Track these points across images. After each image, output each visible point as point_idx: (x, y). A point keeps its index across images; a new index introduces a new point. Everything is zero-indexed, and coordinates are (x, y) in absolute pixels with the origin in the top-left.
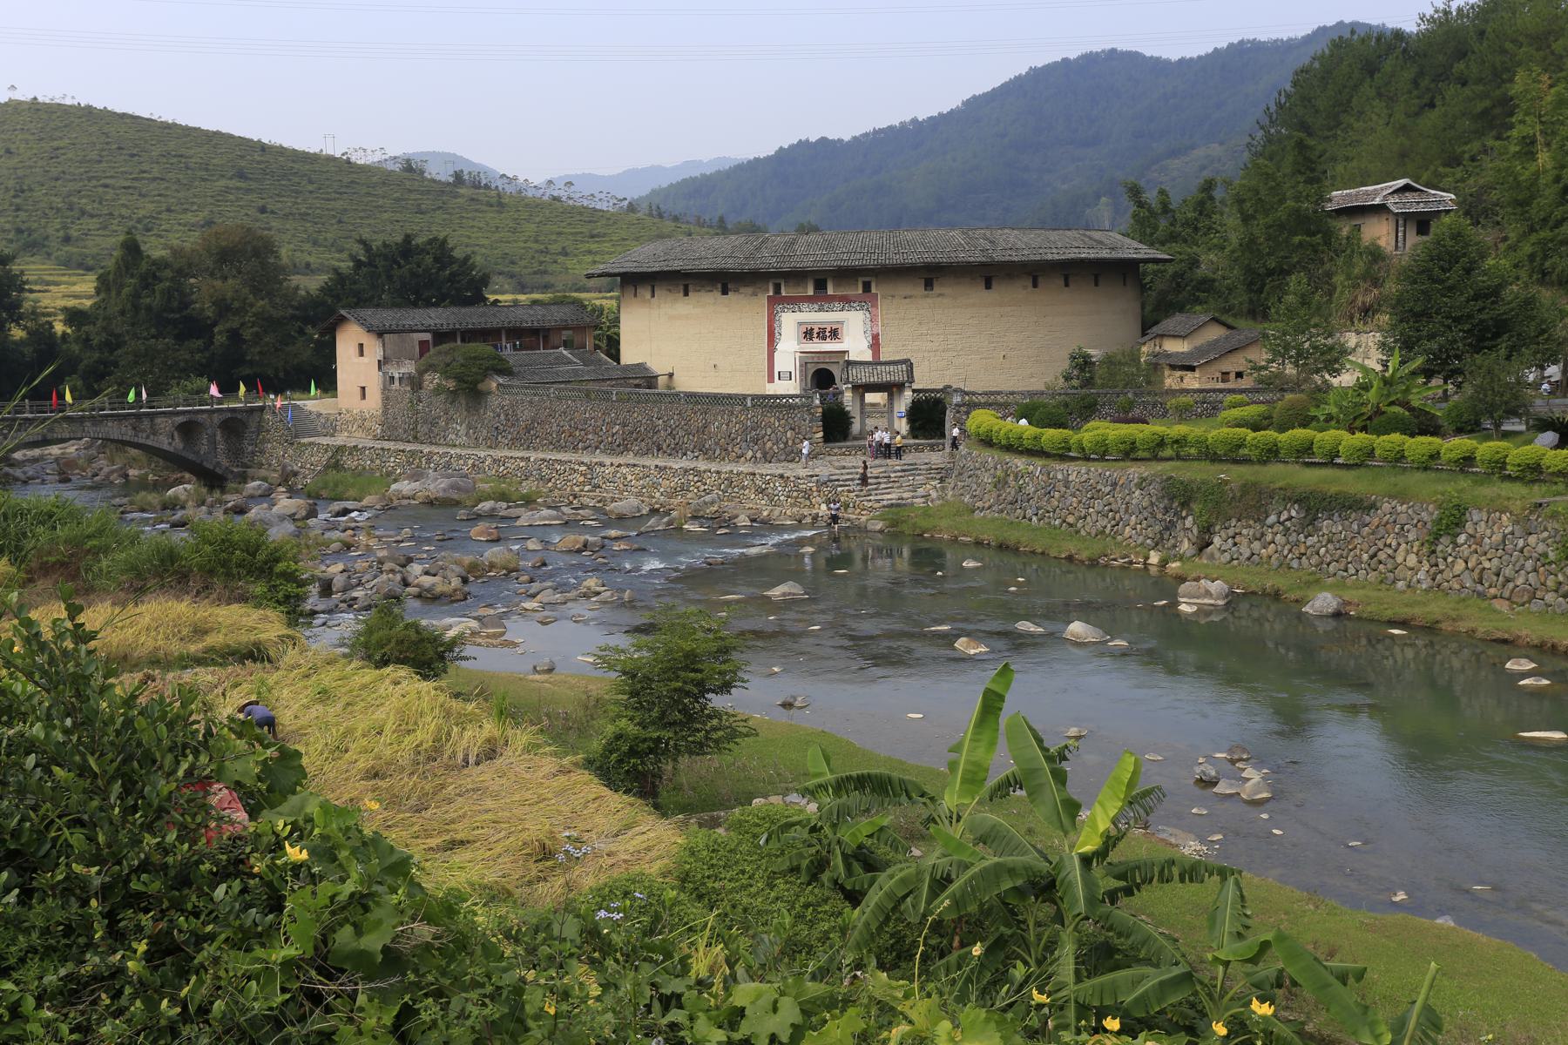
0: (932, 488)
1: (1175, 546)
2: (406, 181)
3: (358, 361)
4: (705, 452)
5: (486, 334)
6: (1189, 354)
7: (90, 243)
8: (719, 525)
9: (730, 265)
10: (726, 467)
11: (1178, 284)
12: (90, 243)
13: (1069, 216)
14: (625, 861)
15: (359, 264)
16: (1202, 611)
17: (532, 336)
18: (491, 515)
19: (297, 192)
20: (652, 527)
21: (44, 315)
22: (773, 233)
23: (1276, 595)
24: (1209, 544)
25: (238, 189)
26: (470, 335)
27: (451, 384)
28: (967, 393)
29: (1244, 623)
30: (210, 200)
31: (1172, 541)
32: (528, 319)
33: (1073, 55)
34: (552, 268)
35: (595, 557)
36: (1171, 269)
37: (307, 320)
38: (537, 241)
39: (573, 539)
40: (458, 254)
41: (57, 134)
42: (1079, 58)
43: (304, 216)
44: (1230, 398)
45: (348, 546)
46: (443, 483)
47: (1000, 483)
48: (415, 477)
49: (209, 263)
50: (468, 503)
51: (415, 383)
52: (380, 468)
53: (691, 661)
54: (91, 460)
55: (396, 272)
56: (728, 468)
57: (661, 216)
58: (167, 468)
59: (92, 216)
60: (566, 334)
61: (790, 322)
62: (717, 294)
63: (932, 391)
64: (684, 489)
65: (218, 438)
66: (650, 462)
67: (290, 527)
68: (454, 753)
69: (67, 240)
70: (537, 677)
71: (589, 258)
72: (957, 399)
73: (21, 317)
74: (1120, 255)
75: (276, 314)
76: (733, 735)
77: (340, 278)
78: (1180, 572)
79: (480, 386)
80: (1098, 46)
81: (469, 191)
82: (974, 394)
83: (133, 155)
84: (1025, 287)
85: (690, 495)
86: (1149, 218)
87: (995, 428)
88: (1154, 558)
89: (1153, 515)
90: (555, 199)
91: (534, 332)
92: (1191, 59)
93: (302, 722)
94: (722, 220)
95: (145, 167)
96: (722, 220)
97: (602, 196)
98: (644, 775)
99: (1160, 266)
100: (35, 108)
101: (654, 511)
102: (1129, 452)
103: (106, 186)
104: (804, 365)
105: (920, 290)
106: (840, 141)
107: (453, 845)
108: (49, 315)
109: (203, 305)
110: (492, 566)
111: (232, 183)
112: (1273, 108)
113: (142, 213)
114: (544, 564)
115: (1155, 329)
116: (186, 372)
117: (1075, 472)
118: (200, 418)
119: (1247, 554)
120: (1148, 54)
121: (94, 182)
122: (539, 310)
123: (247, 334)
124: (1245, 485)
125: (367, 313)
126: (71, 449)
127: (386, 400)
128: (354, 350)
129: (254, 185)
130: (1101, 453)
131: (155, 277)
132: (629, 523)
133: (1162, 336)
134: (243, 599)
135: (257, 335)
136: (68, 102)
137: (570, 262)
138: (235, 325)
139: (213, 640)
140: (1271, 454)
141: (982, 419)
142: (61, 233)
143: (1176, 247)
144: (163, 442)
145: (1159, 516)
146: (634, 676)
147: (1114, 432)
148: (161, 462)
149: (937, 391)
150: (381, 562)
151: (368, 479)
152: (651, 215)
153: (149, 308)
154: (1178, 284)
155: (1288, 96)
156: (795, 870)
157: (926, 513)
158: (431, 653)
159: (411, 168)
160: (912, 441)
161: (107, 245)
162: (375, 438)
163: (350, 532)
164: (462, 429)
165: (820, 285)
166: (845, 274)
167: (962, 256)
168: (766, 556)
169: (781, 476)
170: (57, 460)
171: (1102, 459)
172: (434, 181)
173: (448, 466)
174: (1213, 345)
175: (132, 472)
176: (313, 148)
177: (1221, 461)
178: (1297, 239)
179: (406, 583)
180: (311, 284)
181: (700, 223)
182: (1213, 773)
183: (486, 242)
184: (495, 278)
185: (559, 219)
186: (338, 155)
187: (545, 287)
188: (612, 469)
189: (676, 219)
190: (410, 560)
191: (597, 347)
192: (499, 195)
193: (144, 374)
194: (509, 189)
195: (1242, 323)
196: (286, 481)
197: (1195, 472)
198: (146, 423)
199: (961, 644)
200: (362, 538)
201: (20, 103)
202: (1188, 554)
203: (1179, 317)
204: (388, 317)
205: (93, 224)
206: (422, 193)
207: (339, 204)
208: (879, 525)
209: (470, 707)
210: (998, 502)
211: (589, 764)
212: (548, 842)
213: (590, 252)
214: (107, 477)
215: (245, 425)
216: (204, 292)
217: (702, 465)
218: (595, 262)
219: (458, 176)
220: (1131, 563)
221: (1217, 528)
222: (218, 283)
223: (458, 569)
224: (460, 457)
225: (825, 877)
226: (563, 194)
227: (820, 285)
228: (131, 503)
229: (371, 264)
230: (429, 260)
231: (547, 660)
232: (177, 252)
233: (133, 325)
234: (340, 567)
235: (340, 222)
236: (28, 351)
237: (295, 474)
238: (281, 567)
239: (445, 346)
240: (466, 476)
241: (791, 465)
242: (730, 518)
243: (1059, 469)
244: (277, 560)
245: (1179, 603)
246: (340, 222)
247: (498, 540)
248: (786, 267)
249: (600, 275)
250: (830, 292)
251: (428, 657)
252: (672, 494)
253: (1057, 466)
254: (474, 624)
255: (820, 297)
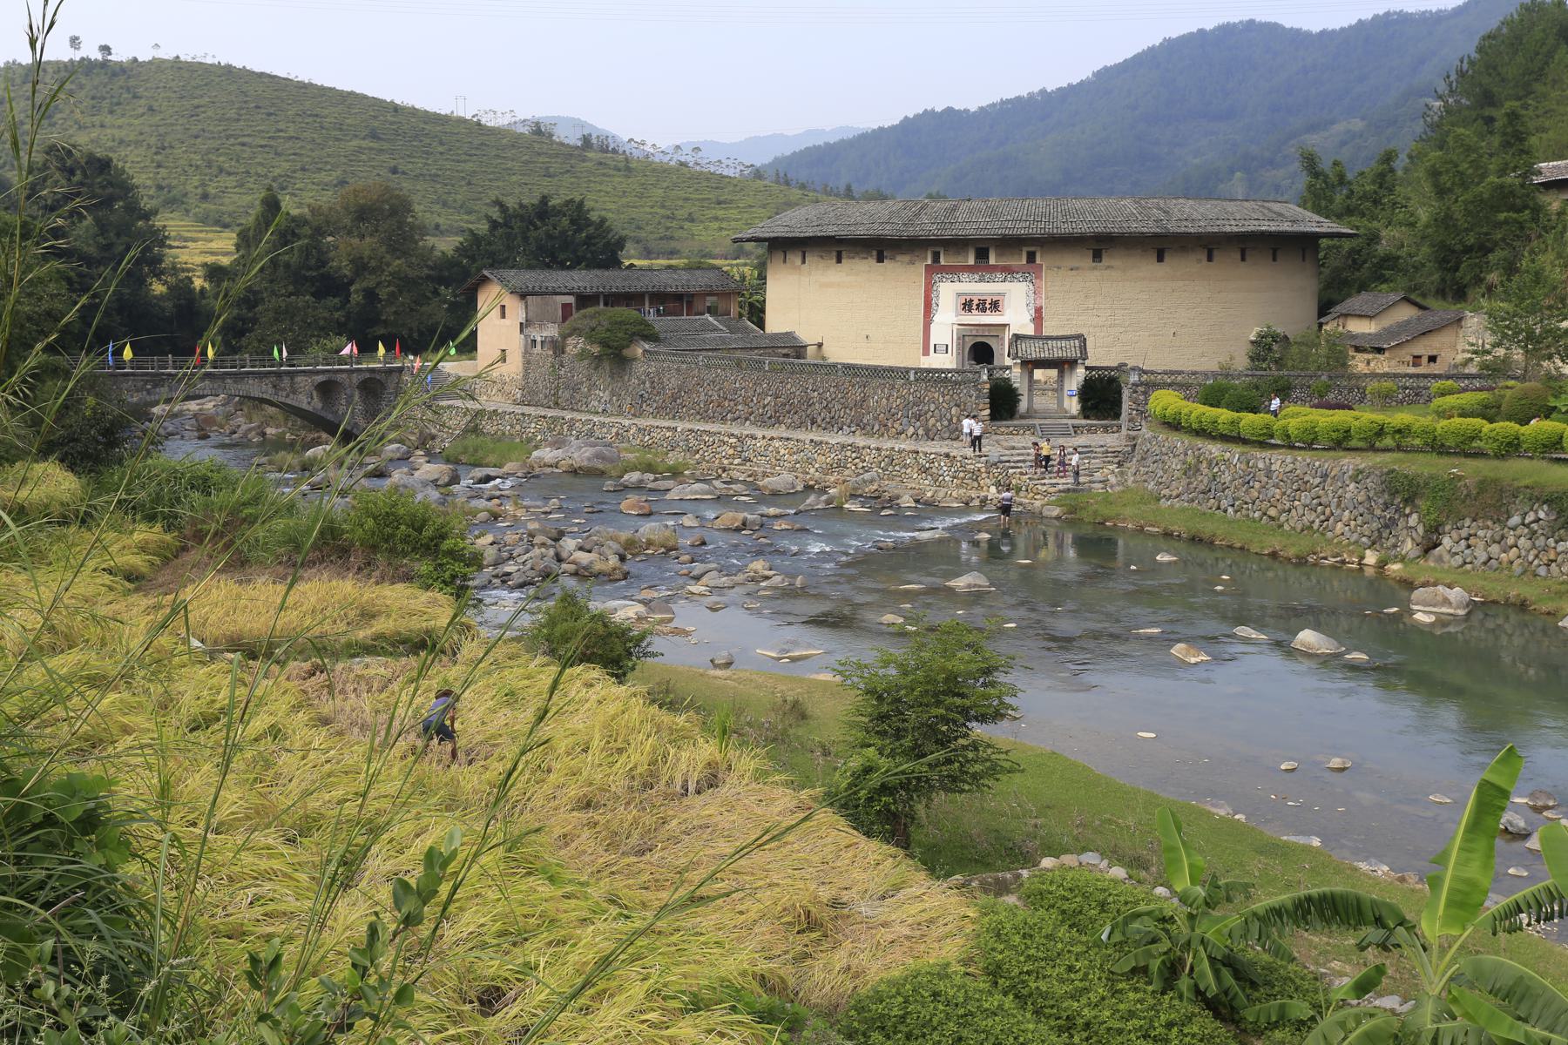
0: (1110, 472)
1: (1395, 546)
2: (536, 141)
3: (502, 328)
4: (862, 427)
5: (630, 298)
6: (1378, 336)
7: (227, 201)
8: (881, 506)
9: (888, 231)
10: (889, 445)
11: (1354, 261)
12: (227, 201)
13: (1204, 187)
14: (908, 938)
15: (494, 225)
16: (1441, 622)
17: (675, 301)
18: (638, 487)
19: (427, 153)
20: (808, 505)
21: (183, 270)
22: (917, 202)
23: (1523, 606)
24: (1436, 546)
25: (371, 149)
26: (613, 299)
27: (596, 349)
28: (1145, 372)
29: (1475, 634)
30: (344, 160)
31: (1392, 540)
32: (673, 283)
33: (1209, 26)
34: (677, 234)
35: (756, 537)
36: (1347, 245)
37: (442, 280)
38: (663, 207)
39: (731, 517)
40: (594, 216)
41: (198, 92)
42: (1215, 29)
43: (434, 178)
44: (1436, 385)
45: (496, 517)
46: (588, 452)
47: (1191, 471)
48: (558, 444)
49: (347, 221)
50: (614, 473)
51: (558, 347)
52: (520, 434)
53: (954, 684)
54: (229, 416)
55: (533, 234)
56: (889, 445)
57: (787, 183)
58: (303, 427)
59: (229, 174)
60: (710, 301)
61: (949, 292)
62: (872, 262)
63: (1106, 368)
64: (841, 465)
65: (357, 398)
66: (806, 436)
67: (434, 494)
68: (672, 779)
69: (205, 197)
70: (719, 673)
71: (715, 225)
72: (1134, 378)
73: (162, 273)
74: (1302, 229)
75: (412, 273)
76: (994, 770)
77: (476, 239)
78: (1405, 575)
79: (626, 352)
80: (1236, 16)
81: (596, 154)
82: (1152, 373)
83: (270, 114)
84: (1199, 261)
85: (847, 472)
86: (1323, 187)
87: (1185, 411)
88: (1371, 558)
89: (1370, 511)
90: (683, 164)
91: (678, 297)
92: (1333, 31)
93: (491, 729)
94: (849, 188)
95: (282, 126)
96: (849, 188)
97: (729, 162)
98: (895, 815)
99: (1335, 242)
100: (177, 66)
101: (809, 488)
102: (1341, 442)
103: (243, 144)
104: (962, 338)
105: (1087, 261)
106: (966, 111)
107: (695, 900)
108: (188, 270)
109: (341, 264)
110: (650, 543)
111: (365, 144)
112: (1453, 77)
113: (277, 171)
114: (704, 543)
115: (1338, 308)
116: (324, 331)
117: (1279, 461)
118: (340, 377)
119: (1484, 558)
120: (1288, 26)
121: (232, 141)
122: (664, 276)
123: (383, 293)
124: (1482, 482)
125: (510, 273)
126: (209, 405)
127: (527, 363)
128: (496, 312)
129: (386, 146)
130: (1310, 441)
131: (294, 234)
132: (782, 500)
133: (1346, 316)
134: (408, 578)
135: (392, 294)
136: (209, 61)
137: (697, 228)
138: (372, 284)
139: (382, 625)
140: (1511, 448)
141: (1165, 401)
142: (200, 191)
143: (1355, 220)
144: (303, 401)
145: (1378, 512)
146: (880, 698)
147: (1326, 419)
148: (299, 422)
149: (1112, 369)
150: (532, 535)
151: (507, 445)
152: (777, 182)
153: (287, 265)
154: (1354, 261)
155: (1472, 63)
156: (1140, 971)
157: (1107, 500)
158: (619, 650)
159: (540, 131)
160: (1084, 422)
161: (246, 202)
162: (515, 403)
163: (496, 501)
164: (606, 396)
165: (982, 254)
166: (1009, 243)
167: (1135, 227)
168: (940, 541)
169: (947, 456)
170: (195, 416)
171: (1309, 446)
172: (562, 144)
173: (590, 433)
174: (1403, 326)
175: (269, 431)
176: (444, 110)
177: (1449, 454)
178: (1502, 216)
179: (559, 559)
180: (446, 245)
181: (828, 192)
182: (1522, 824)
183: (613, 207)
184: (629, 245)
185: (688, 185)
186: (468, 117)
187: (672, 253)
188: (763, 442)
189: (803, 187)
190: (561, 534)
191: (741, 315)
192: (627, 159)
193: (283, 332)
194: (636, 153)
195: (1430, 302)
196: (424, 444)
197: (1422, 466)
198: (286, 381)
199: (1178, 650)
200: (509, 507)
201: (163, 61)
202: (1412, 555)
203: (1364, 295)
204: (531, 278)
205: (230, 181)
206: (550, 156)
207: (469, 166)
208: (1056, 512)
209: (681, 720)
210: (1187, 490)
211: (831, 799)
212: (813, 910)
213: (716, 219)
214: (245, 435)
215: (383, 386)
216: (342, 250)
217: (860, 441)
218: (721, 229)
219: (586, 140)
220: (1343, 562)
221: (1448, 528)
222: (355, 241)
223: (615, 546)
224: (603, 425)
225: (1184, 983)
226: (690, 160)
227: (982, 254)
228: (270, 463)
229: (506, 225)
230: (565, 222)
231: (725, 653)
232: (314, 211)
233: (272, 281)
234: (489, 538)
235: (469, 183)
236: (169, 304)
237: (433, 437)
238: (447, 544)
239: (591, 310)
240: (610, 445)
241: (956, 444)
242: (891, 500)
243: (1260, 457)
244: (443, 537)
245: (1411, 613)
246: (469, 183)
247: (650, 514)
248: (948, 234)
249: (749, 240)
250: (992, 261)
251: (613, 652)
252: (829, 469)
253: (1258, 453)
254: (641, 608)
255: (981, 266)
